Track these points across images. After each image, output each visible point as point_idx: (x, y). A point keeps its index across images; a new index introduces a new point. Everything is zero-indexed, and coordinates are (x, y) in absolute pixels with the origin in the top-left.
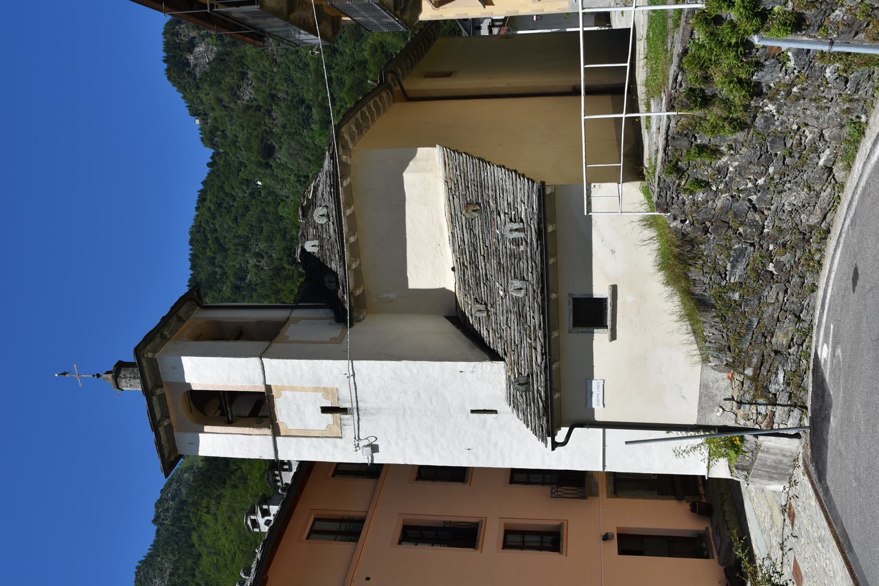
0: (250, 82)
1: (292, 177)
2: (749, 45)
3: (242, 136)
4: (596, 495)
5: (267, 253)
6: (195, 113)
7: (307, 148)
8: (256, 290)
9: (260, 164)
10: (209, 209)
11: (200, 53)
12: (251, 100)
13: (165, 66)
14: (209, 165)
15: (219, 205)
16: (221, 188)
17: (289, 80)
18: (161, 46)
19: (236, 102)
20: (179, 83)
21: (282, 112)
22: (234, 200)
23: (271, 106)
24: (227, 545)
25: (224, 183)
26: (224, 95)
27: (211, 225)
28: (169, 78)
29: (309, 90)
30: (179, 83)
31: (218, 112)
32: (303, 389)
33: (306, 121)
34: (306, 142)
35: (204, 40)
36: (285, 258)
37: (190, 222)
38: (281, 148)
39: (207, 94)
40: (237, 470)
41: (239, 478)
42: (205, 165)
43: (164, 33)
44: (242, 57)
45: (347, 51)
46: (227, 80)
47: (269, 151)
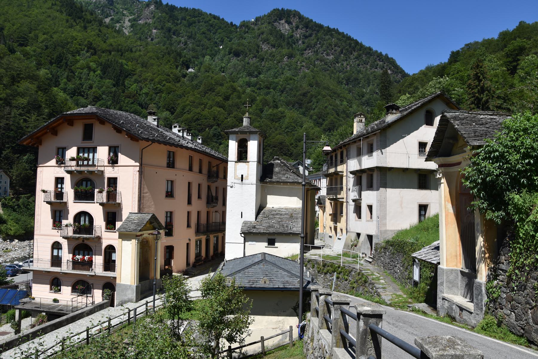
0: (270, 49)
1: (224, 65)
2: (334, 272)
3: (245, 42)
4: (196, 236)
5: (186, 47)
6: (257, 19)
7: (238, 74)
8: (168, 40)
9: (231, 49)
10: (210, 20)
11: (285, 26)
12: (262, 49)
13: (280, 9)
14: (232, 23)
15: (212, 26)
16: (220, 28)
17: (269, 69)
18: (289, 8)
19: (261, 41)
20: (272, 14)
21: (255, 63)
22: (214, 34)
23: (258, 58)
24: (34, 13)
25: (222, 29)
26: (265, 35)
27: (202, 20)
28: (274, 10)
29: (265, 77)
30: (272, 14)
31: (257, 32)
32: (248, 171)
33: (250, 75)
34: (240, 73)
35: (291, 29)
36: (185, 59)
37: (204, 10)
38: (238, 60)
39: (265, 27)
40: (76, 23)
41: (72, 24)
42: (231, 21)
43: (295, 10)
44: (282, 47)
45: (282, 98)
46: (272, 38)
47: (237, 54)
